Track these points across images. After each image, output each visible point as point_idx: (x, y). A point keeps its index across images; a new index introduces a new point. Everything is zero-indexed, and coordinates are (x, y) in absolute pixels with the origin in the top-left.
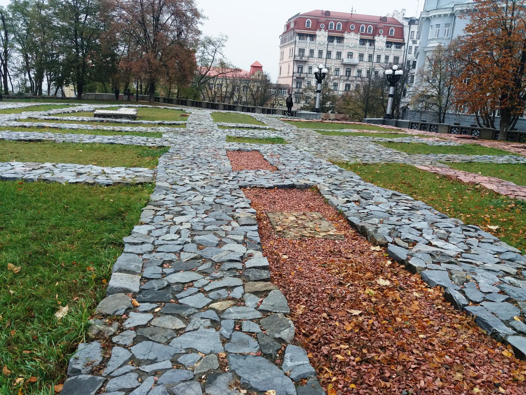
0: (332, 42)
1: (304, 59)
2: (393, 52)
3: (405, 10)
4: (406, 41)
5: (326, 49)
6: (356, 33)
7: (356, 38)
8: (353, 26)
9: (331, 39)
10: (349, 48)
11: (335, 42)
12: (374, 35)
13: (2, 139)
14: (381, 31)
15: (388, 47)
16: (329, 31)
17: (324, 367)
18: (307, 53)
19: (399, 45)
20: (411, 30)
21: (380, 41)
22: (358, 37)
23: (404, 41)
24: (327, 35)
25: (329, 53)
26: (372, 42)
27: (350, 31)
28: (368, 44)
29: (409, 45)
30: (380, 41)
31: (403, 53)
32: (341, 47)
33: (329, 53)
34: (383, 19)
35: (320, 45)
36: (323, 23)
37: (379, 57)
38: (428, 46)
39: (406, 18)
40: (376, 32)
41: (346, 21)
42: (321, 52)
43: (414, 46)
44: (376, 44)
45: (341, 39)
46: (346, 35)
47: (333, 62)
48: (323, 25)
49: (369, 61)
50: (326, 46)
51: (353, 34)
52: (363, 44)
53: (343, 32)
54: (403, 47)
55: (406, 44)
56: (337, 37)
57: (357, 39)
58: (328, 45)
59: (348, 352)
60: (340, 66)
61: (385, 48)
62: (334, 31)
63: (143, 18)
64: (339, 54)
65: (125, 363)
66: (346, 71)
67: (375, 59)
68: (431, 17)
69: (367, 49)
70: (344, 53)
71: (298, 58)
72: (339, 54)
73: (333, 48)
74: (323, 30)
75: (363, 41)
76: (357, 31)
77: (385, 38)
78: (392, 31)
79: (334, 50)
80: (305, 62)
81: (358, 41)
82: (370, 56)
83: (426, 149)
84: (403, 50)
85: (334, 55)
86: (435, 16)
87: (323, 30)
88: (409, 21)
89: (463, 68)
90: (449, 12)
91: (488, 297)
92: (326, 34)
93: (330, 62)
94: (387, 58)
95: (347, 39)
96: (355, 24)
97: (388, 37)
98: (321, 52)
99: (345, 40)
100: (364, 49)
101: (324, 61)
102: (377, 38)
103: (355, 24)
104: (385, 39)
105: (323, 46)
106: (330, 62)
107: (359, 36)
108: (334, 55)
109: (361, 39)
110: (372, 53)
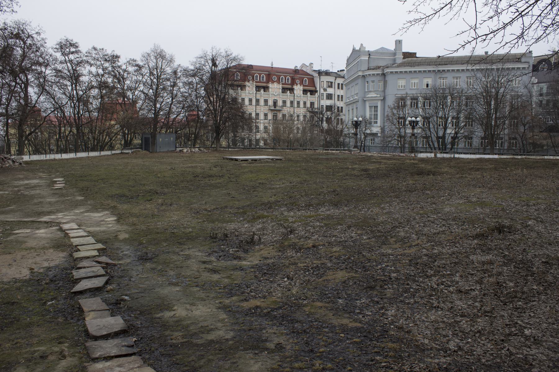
0: (306, 94)
1: (277, 108)
2: (309, 98)
3: (312, 64)
4: (318, 89)
5: (254, 97)
6: (279, 83)
7: (278, 87)
8: (275, 78)
10: (274, 96)
11: (262, 91)
14: (298, 81)
15: (303, 94)
16: (304, 86)
18: (280, 103)
19: (313, 92)
20: (321, 81)
21: (298, 89)
22: (280, 86)
23: (316, 88)
24: (302, 89)
25: (258, 101)
26: (292, 90)
27: (273, 82)
28: (309, 93)
30: (298, 89)
31: (317, 99)
32: (267, 96)
33: (258, 101)
34: (296, 71)
35: (249, 95)
36: (297, 79)
37: (298, 103)
38: (367, 96)
39: (314, 71)
40: (293, 82)
41: (267, 73)
43: (325, 93)
44: (295, 92)
45: (266, 89)
46: (270, 85)
47: (262, 108)
49: (291, 107)
50: (255, 95)
51: (275, 85)
52: (259, 91)
53: (268, 82)
54: (317, 94)
55: (319, 92)
57: (280, 89)
58: (256, 94)
60: (267, 111)
61: (302, 95)
62: (260, 82)
64: (266, 101)
66: (273, 116)
68: (366, 75)
69: (288, 96)
70: (270, 101)
71: (273, 108)
72: (266, 101)
73: (261, 96)
74: (299, 85)
75: (284, 90)
76: (278, 82)
77: (302, 87)
79: (262, 98)
80: (280, 111)
82: (292, 103)
84: (317, 96)
85: (262, 102)
86: (369, 75)
87: (299, 85)
88: (318, 72)
92: (302, 88)
94: (305, 103)
95: (271, 88)
96: (276, 75)
98: (250, 100)
99: (270, 89)
100: (286, 97)
101: (254, 108)
102: (295, 87)
103: (276, 75)
105: (252, 95)
107: (281, 86)
108: (262, 102)
110: (292, 100)
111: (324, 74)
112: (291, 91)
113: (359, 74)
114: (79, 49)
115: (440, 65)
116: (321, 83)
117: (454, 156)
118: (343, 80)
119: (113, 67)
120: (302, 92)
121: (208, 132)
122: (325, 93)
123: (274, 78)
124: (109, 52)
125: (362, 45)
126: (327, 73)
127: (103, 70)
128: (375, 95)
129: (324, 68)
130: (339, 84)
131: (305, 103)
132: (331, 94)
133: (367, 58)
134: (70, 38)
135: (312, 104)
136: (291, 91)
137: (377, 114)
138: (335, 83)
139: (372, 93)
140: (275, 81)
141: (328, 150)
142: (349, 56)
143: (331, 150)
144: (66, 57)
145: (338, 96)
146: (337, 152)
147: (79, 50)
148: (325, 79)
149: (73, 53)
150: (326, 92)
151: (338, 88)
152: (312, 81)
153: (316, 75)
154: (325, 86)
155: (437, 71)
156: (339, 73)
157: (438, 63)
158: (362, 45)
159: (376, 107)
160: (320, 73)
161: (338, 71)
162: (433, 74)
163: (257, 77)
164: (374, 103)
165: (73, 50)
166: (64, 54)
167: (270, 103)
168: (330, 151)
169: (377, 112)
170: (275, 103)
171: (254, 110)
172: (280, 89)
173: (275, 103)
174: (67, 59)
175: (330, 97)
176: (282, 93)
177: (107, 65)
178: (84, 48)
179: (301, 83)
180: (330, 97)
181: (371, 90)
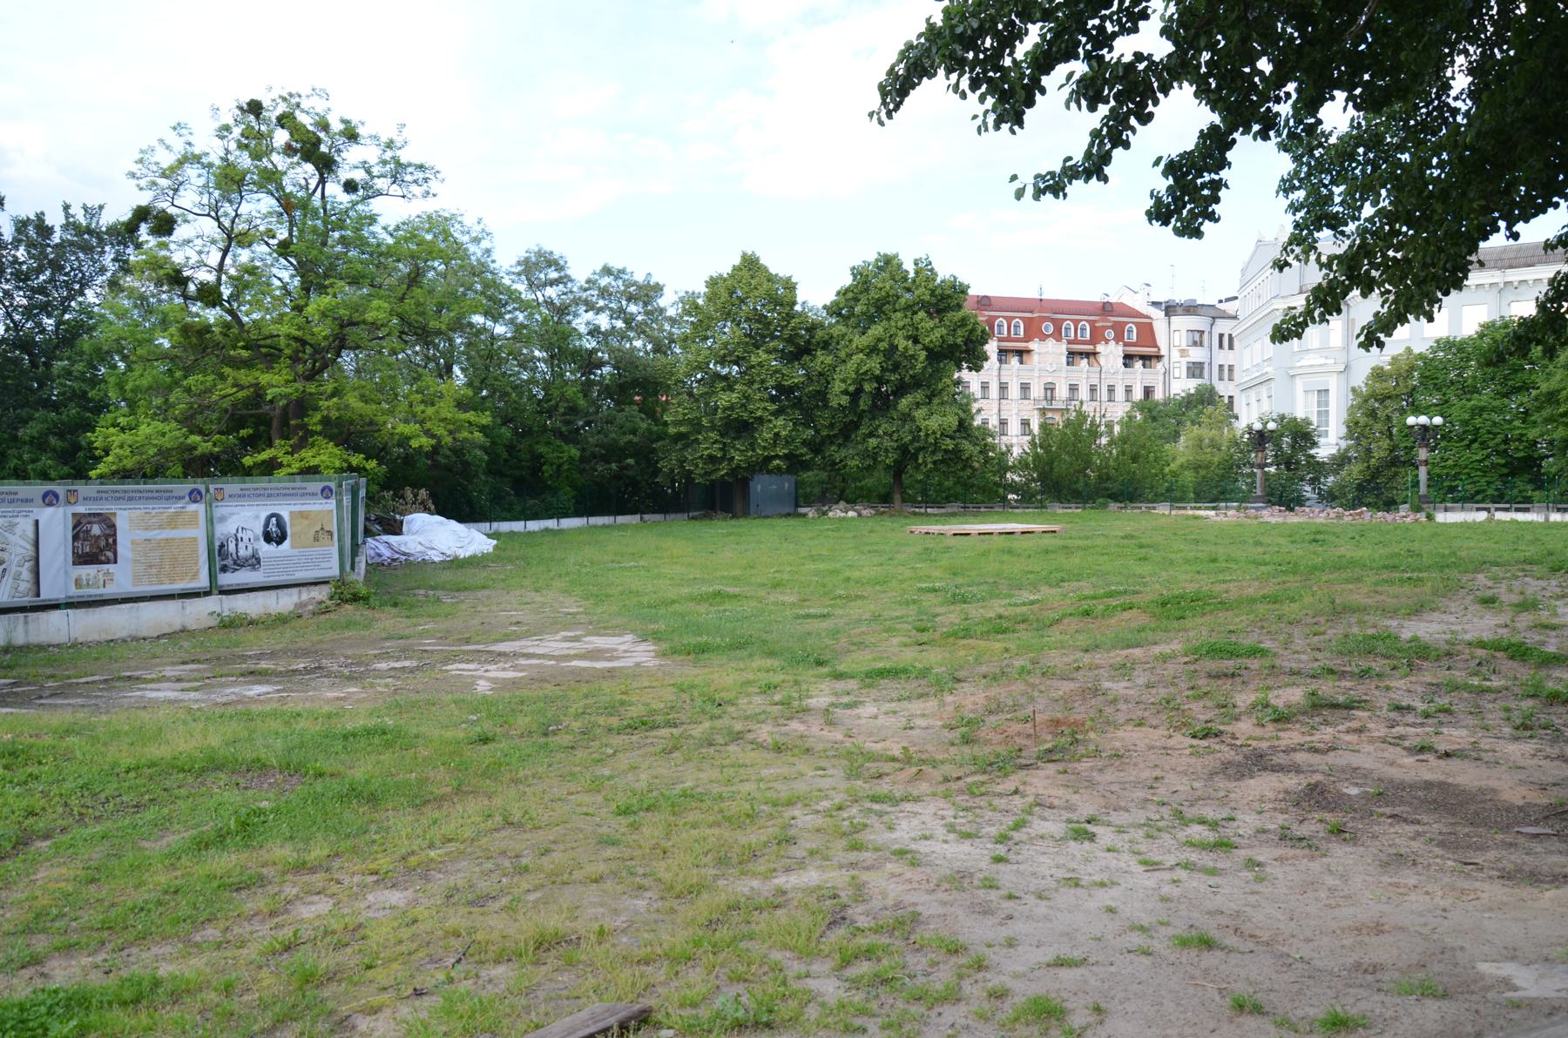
2: (1139, 376)
5: (996, 379)
6: (1059, 339)
13: (7, 650)
15: (1126, 365)
16: (1126, 345)
17: (714, 872)
20: (1173, 328)
21: (1111, 353)
22: (1063, 348)
25: (1003, 388)
27: (1043, 338)
30: (1111, 353)
37: (1111, 389)
38: (1299, 364)
39: (1154, 304)
40: (1097, 336)
43: (1184, 361)
44: (1102, 360)
48: (1110, 334)
53: (1027, 339)
57: (1061, 354)
59: (516, 318)
62: (1008, 339)
63: (733, 705)
72: (1025, 388)
76: (1057, 336)
78: (1130, 331)
85: (1014, 391)
89: (510, 312)
94: (1128, 390)
96: (1053, 321)
103: (1053, 321)
108: (1014, 391)
111: (1179, 310)
112: (1092, 358)
113: (1275, 307)
114: (569, 272)
115: (1511, 267)
116: (1172, 336)
117: (1547, 519)
118: (1233, 323)
119: (647, 313)
120: (1121, 361)
121: (325, 223)
123: (1046, 328)
124: (639, 277)
126: (1191, 309)
127: (626, 321)
128: (1322, 361)
129: (1180, 297)
130: (1221, 336)
131: (1128, 390)
132: (1201, 364)
134: (547, 248)
135: (1148, 391)
136: (1092, 358)
137: (1327, 412)
138: (1210, 333)
139: (1311, 356)
140: (1049, 336)
141: (1185, 508)
142: (1246, 260)
143: (1192, 508)
144: (539, 294)
145: (1221, 366)
146: (128, 674)
147: (567, 276)
148: (1182, 323)
149: (552, 283)
151: (1221, 346)
152: (1147, 333)
153: (1158, 315)
154: (1184, 346)
155: (1502, 285)
156: (1221, 306)
157: (1506, 263)
159: (1324, 392)
160: (1170, 309)
161: (1221, 301)
162: (1495, 291)
163: (1000, 326)
164: (1319, 382)
165: (553, 275)
166: (531, 285)
167: (1037, 391)
168: (1190, 512)
169: (1327, 405)
170: (1050, 389)
171: (996, 411)
172: (1061, 354)
173: (1050, 389)
174: (541, 299)
175: (1197, 372)
176: (1068, 364)
177: (633, 308)
178: (580, 272)
179: (1119, 338)
180: (1197, 372)
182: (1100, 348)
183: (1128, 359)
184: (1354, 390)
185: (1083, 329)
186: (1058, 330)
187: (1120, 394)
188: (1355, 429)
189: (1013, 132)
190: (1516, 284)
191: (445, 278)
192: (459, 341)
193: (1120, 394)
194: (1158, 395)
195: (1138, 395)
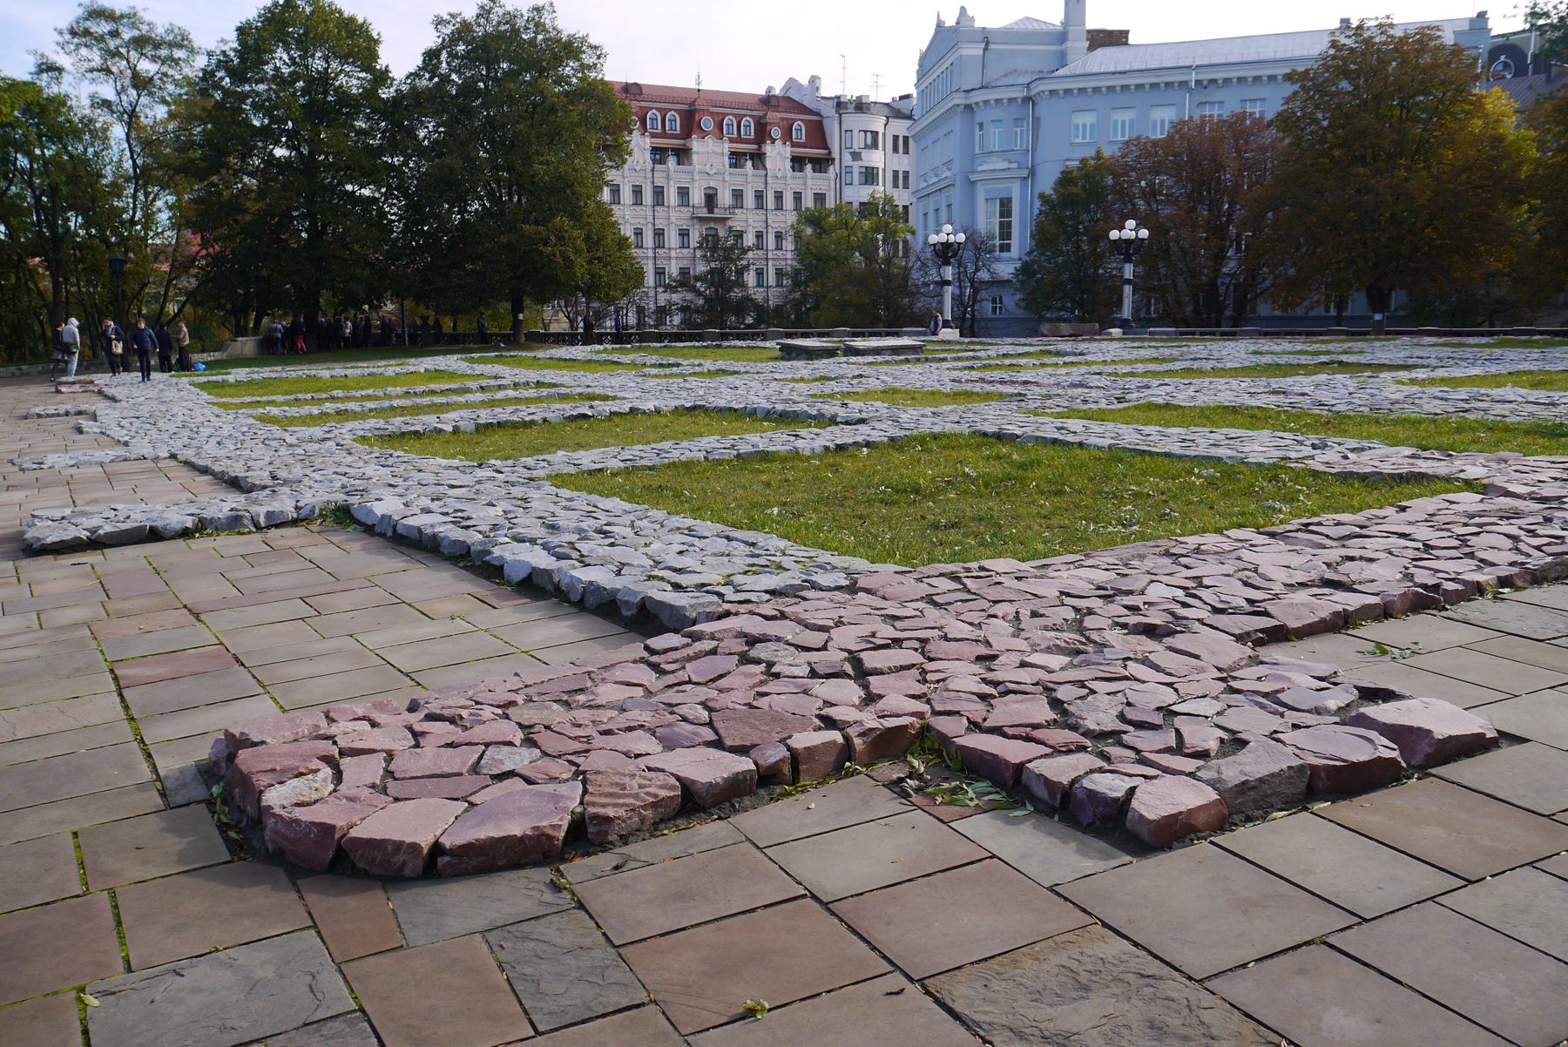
0: (801, 170)
2: (812, 182)
4: (836, 155)
7: (718, 150)
8: (707, 123)
9: (659, 154)
11: (672, 161)
12: (686, 134)
18: (725, 198)
19: (821, 164)
20: (844, 128)
21: (777, 154)
22: (726, 147)
23: (830, 153)
25: (659, 193)
27: (703, 134)
29: (845, 163)
33: (659, 193)
37: (779, 196)
38: (980, 169)
42: (637, 191)
44: (769, 163)
45: (683, 154)
50: (649, 175)
52: (662, 161)
54: (831, 168)
55: (837, 162)
56: (673, 150)
58: (653, 170)
61: (789, 173)
62: (664, 135)
65: (1208, 587)
67: (648, 196)
68: (977, 104)
75: (737, 159)
81: (726, 159)
82: (759, 196)
83: (1305, 353)
85: (672, 197)
86: (986, 102)
90: (1019, 94)
91: (1036, 996)
93: (743, 216)
94: (798, 197)
95: (697, 153)
96: (712, 114)
97: (653, 136)
99: (694, 157)
103: (712, 114)
104: (788, 151)
105: (642, 174)
106: (743, 216)
108: (672, 197)
109: (732, 153)
120: (789, 164)
122: (856, 164)
125: (963, 9)
128: (1005, 165)
130: (896, 138)
133: (980, 52)
135: (820, 198)
139: (994, 159)
150: (860, 163)
151: (895, 150)
158: (963, 9)
164: (1000, 189)
167: (697, 197)
170: (711, 199)
181: (992, 149)
182: (696, 144)
183: (798, 162)
184: (1041, 196)
185: (673, 121)
186: (720, 126)
187: (789, 202)
188: (1043, 238)
189: (80, 5)
190: (1205, 83)
191: (534, 108)
192: (778, 791)
193: (789, 202)
194: (830, 204)
195: (808, 202)
